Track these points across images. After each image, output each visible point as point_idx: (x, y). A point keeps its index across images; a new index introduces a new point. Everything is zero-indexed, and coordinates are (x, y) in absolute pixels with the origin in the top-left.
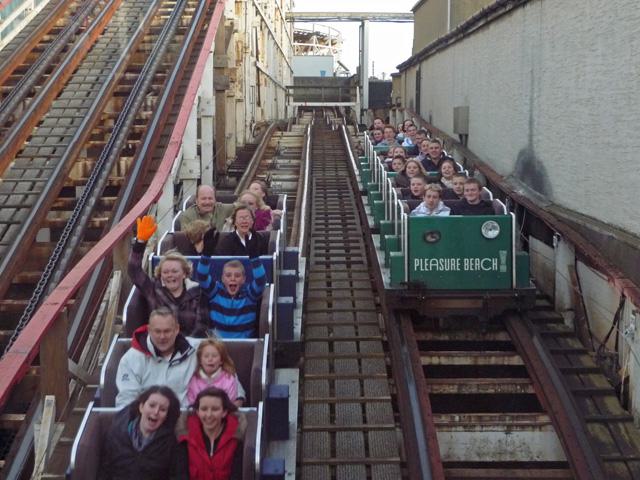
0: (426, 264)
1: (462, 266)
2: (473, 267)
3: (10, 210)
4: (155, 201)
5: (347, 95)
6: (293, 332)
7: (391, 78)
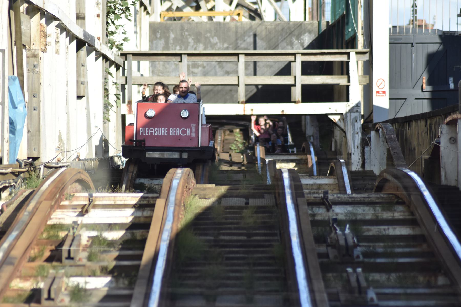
0: (147, 131)
2: (175, 133)
3: (402, 100)
4: (32, 79)
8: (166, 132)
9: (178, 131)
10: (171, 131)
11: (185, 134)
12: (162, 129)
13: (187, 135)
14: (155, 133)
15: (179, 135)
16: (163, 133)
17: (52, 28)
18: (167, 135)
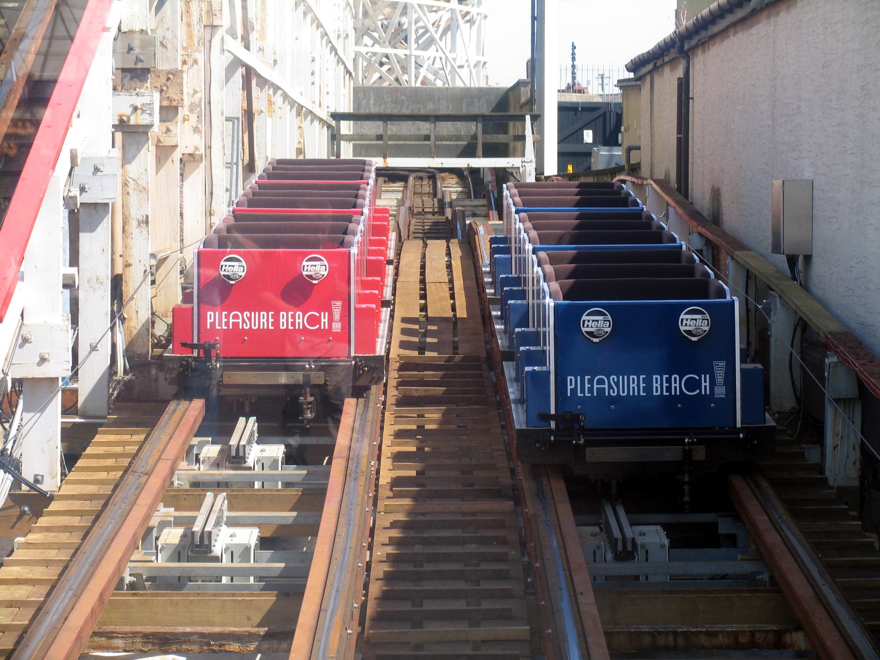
0: (224, 320)
1: (276, 323)
2: (293, 324)
5: (501, 138)
6: (421, 471)
7: (617, 91)
8: (271, 320)
9: (675, 383)
10: (283, 318)
11: (318, 326)
12: (262, 313)
13: (322, 328)
14: (245, 325)
15: (301, 328)
16: (263, 322)
17: (278, 99)
18: (273, 328)
